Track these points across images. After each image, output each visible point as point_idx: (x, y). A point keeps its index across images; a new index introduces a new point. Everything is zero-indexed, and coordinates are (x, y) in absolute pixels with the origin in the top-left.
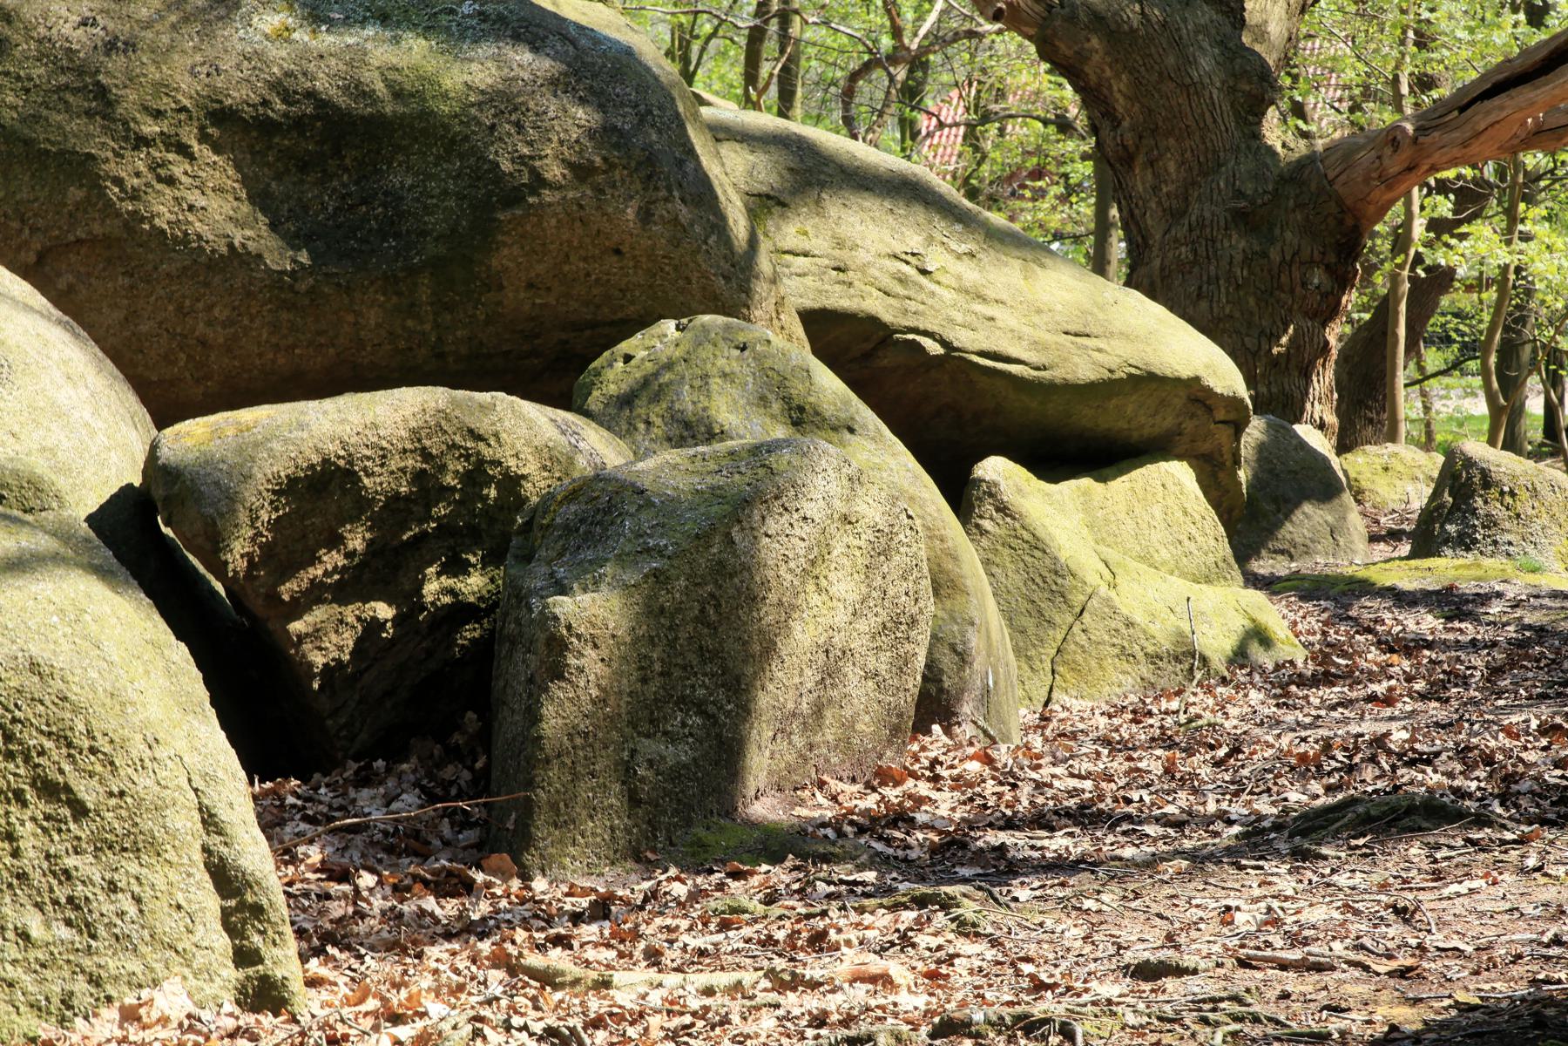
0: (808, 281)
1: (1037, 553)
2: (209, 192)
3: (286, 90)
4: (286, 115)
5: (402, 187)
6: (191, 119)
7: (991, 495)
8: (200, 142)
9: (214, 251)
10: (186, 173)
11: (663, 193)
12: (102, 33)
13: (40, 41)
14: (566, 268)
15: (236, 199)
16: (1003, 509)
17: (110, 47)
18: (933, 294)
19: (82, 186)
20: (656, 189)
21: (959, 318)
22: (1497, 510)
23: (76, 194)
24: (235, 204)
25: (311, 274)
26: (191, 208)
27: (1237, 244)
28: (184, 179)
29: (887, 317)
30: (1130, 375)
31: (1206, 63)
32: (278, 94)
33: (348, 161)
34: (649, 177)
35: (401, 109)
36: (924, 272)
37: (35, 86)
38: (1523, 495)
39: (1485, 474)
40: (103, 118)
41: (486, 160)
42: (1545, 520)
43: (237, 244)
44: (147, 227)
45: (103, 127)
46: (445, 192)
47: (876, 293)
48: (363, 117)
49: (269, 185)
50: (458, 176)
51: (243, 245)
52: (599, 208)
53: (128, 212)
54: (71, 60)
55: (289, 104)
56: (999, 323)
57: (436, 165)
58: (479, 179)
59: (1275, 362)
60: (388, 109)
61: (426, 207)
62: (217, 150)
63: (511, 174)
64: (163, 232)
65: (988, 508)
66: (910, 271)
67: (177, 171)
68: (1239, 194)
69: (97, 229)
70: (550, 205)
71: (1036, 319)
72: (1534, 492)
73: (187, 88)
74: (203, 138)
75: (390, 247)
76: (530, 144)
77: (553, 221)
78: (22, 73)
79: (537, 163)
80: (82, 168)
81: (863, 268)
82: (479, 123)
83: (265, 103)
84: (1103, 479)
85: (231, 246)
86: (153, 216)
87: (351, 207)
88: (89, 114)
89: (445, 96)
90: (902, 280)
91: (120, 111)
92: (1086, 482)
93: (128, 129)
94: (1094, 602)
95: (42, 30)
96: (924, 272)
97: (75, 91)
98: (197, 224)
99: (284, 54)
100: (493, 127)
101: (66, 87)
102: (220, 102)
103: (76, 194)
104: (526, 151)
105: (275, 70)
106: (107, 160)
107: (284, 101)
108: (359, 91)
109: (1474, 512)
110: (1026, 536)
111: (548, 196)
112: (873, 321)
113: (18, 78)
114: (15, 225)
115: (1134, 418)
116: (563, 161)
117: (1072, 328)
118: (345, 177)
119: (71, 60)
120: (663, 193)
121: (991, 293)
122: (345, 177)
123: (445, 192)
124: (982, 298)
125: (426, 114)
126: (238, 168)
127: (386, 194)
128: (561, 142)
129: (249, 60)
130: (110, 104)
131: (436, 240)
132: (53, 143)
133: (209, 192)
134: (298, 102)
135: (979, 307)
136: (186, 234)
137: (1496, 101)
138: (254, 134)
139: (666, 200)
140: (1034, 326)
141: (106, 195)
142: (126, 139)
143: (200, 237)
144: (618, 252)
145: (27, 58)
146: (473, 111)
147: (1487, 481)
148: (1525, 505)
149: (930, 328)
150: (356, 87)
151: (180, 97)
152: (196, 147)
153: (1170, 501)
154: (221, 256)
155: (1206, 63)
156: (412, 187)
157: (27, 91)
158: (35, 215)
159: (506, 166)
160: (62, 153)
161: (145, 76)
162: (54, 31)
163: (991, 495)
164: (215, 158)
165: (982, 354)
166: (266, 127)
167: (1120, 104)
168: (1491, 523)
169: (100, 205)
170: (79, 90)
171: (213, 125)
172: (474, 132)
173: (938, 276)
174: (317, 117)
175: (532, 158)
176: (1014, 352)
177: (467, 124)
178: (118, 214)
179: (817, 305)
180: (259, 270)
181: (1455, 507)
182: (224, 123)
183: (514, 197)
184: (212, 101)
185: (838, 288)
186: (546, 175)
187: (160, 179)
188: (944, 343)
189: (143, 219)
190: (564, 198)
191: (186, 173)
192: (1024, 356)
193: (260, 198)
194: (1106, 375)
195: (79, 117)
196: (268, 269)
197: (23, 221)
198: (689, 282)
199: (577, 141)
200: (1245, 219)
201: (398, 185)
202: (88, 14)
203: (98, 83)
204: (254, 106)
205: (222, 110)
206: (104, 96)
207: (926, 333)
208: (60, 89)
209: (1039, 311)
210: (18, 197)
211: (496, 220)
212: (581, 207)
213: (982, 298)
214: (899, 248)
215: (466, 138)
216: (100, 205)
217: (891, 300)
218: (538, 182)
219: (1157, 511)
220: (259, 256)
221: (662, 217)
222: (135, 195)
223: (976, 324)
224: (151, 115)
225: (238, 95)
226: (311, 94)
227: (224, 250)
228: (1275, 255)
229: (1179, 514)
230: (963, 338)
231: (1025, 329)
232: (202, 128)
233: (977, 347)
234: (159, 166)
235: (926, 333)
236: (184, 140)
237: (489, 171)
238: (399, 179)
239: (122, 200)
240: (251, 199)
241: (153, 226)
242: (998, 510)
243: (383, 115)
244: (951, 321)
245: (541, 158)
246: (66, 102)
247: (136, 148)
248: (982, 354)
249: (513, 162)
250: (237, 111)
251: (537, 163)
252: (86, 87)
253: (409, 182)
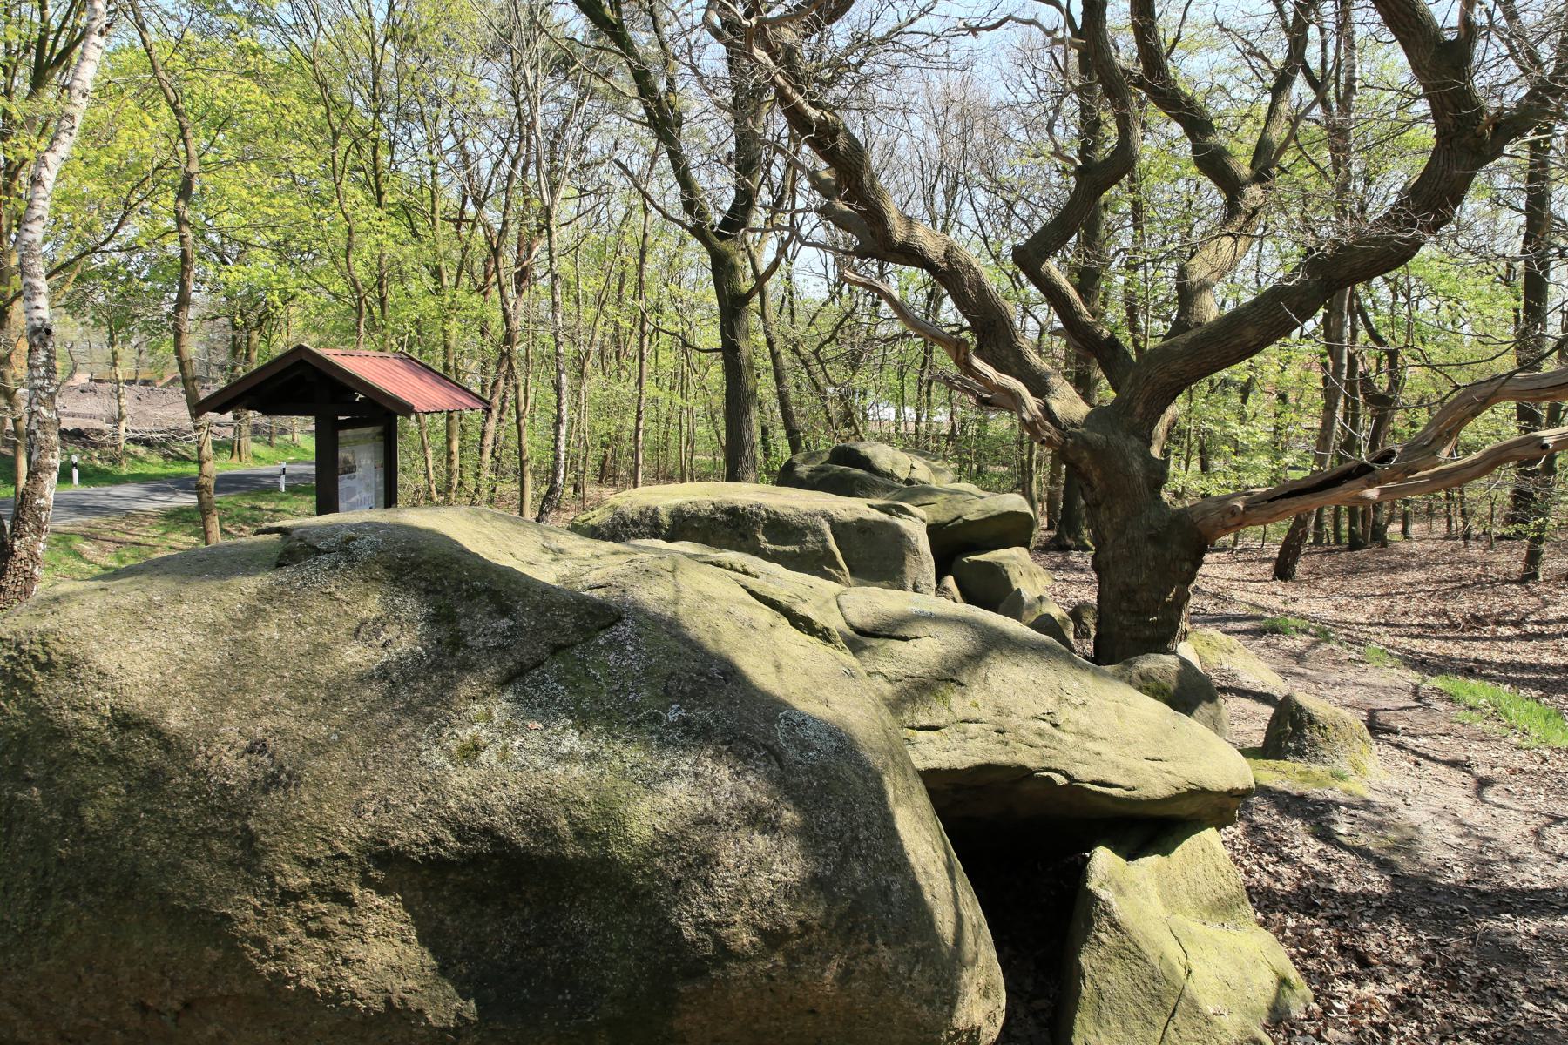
0: (978, 742)
1: (1140, 962)
2: (371, 940)
3: (461, 826)
4: (460, 853)
5: (583, 931)
6: (350, 864)
7: (1106, 913)
8: (362, 886)
9: (368, 1009)
10: (343, 922)
11: (866, 945)
12: (268, 762)
13: (195, 775)
14: (756, 1026)
15: (403, 941)
16: (1115, 925)
17: (272, 782)
18: (1061, 740)
19: (218, 946)
20: (858, 943)
21: (1077, 756)
22: (1317, 737)
23: (212, 954)
24: (402, 946)
25: (476, 1030)
26: (346, 961)
27: (1150, 550)
28: (340, 929)
29: (1031, 764)
30: (1190, 790)
31: (1137, 466)
32: (452, 830)
33: (528, 896)
34: (850, 930)
35: (582, 851)
36: (1055, 725)
37: (181, 828)
38: (1330, 728)
39: (1310, 717)
40: (248, 870)
41: (667, 922)
42: (1342, 742)
43: (395, 999)
44: (292, 987)
45: (245, 881)
46: (624, 948)
47: (1024, 747)
48: (541, 858)
49: (442, 922)
50: (639, 932)
51: (402, 1000)
52: (791, 977)
53: (270, 974)
54: (224, 798)
55: (464, 841)
56: (1104, 757)
57: (617, 915)
58: (660, 943)
59: (1166, 605)
60: (569, 852)
61: (603, 961)
62: (382, 891)
63: (694, 943)
64: (311, 991)
65: (1104, 923)
66: (1045, 726)
67: (331, 922)
68: (1152, 527)
69: (238, 988)
70: (736, 979)
71: (1127, 750)
72: (1336, 727)
73: (350, 831)
74: (366, 882)
75: (564, 1001)
76: (717, 906)
77: (740, 994)
78: (169, 813)
79: (724, 932)
80: (217, 927)
81: (1015, 730)
82: (663, 877)
83: (437, 841)
84: (1166, 852)
85: (388, 1002)
86: (299, 976)
87: (529, 947)
88: (232, 864)
89: (629, 842)
90: (1041, 734)
91: (267, 863)
92: (1155, 860)
93: (273, 884)
94: (1182, 1004)
95: (200, 760)
96: (1055, 725)
97: (222, 836)
98: (353, 979)
99: (464, 781)
100: (678, 883)
101: (214, 831)
102: (386, 844)
103: (212, 954)
104: (712, 915)
105: (452, 803)
106: (246, 920)
107: (458, 838)
108: (541, 829)
109: (1304, 737)
110: (1133, 949)
111: (737, 970)
112: (1022, 768)
113: (164, 818)
114: (156, 975)
115: (1187, 809)
116: (754, 926)
117: (1150, 755)
118: (526, 911)
119: (224, 798)
120: (866, 945)
121: (1097, 733)
122: (526, 911)
123: (624, 948)
124: (1092, 738)
125: (607, 862)
126: (408, 908)
127: (566, 936)
128: (753, 904)
129: (425, 790)
130: (256, 854)
131: (613, 1000)
132: (188, 900)
133: (371, 940)
134: (474, 839)
135: (1090, 745)
136: (339, 991)
137: (1290, 500)
138: (426, 872)
139: (869, 952)
140: (1126, 756)
141: (243, 958)
142: (270, 895)
143: (353, 994)
144: (813, 1012)
145: (178, 795)
146: (658, 861)
147: (1311, 720)
148: (1331, 734)
149: (1059, 766)
150: (537, 824)
151: (337, 843)
152: (356, 891)
153: (1207, 862)
154: (377, 1013)
155: (1137, 466)
156: (592, 933)
157: (172, 834)
158: (175, 968)
159: (689, 933)
160: (195, 912)
161: (301, 818)
162: (213, 762)
163: (1106, 913)
164: (381, 901)
165: (1093, 783)
166: (436, 865)
167: (1095, 481)
168: (1314, 744)
169: (238, 967)
170: (225, 835)
171: (377, 867)
172: (657, 887)
173: (1064, 727)
174: (494, 855)
175: (718, 925)
176: (1114, 779)
177: (650, 877)
178: (258, 975)
179: (983, 762)
180: (418, 1026)
181: (1293, 733)
182: (387, 865)
183: (696, 969)
184: (377, 842)
185: (998, 746)
186: (733, 946)
187: (310, 934)
188: (1068, 776)
189: (287, 980)
190: (752, 972)
191: (343, 922)
192: (1121, 782)
193: (430, 937)
194: (1174, 791)
195: (222, 868)
196: (429, 1026)
197: (163, 973)
198: (890, 1020)
199: (771, 903)
200: (1155, 539)
201: (578, 929)
202: (259, 736)
203: (246, 828)
204: (424, 846)
205: (387, 852)
206: (251, 845)
207: (1056, 771)
208: (205, 833)
209: (1129, 744)
210: (156, 949)
211: (675, 991)
212: (772, 979)
213: (1092, 738)
214: (1039, 711)
215: (649, 894)
216: (238, 967)
217: (1034, 751)
218: (724, 952)
219: (1199, 870)
220: (420, 1012)
221: (863, 972)
222: (279, 956)
223: (1090, 760)
224: (303, 865)
225: (406, 836)
226: (488, 831)
227: (381, 1007)
228: (1168, 556)
229: (1213, 870)
230: (1082, 773)
231: (1122, 760)
232: (364, 872)
233: (1090, 778)
234: (309, 919)
235: (1056, 771)
236: (343, 888)
237: (670, 937)
238: (579, 922)
239: (263, 961)
240: (422, 940)
241: (299, 987)
242: (1111, 925)
243: (564, 858)
244: (1073, 759)
245: (728, 925)
246: (210, 850)
247: (282, 903)
248: (1093, 783)
249: (697, 929)
250: (405, 852)
251: (724, 932)
252: (233, 832)
253: (589, 927)
